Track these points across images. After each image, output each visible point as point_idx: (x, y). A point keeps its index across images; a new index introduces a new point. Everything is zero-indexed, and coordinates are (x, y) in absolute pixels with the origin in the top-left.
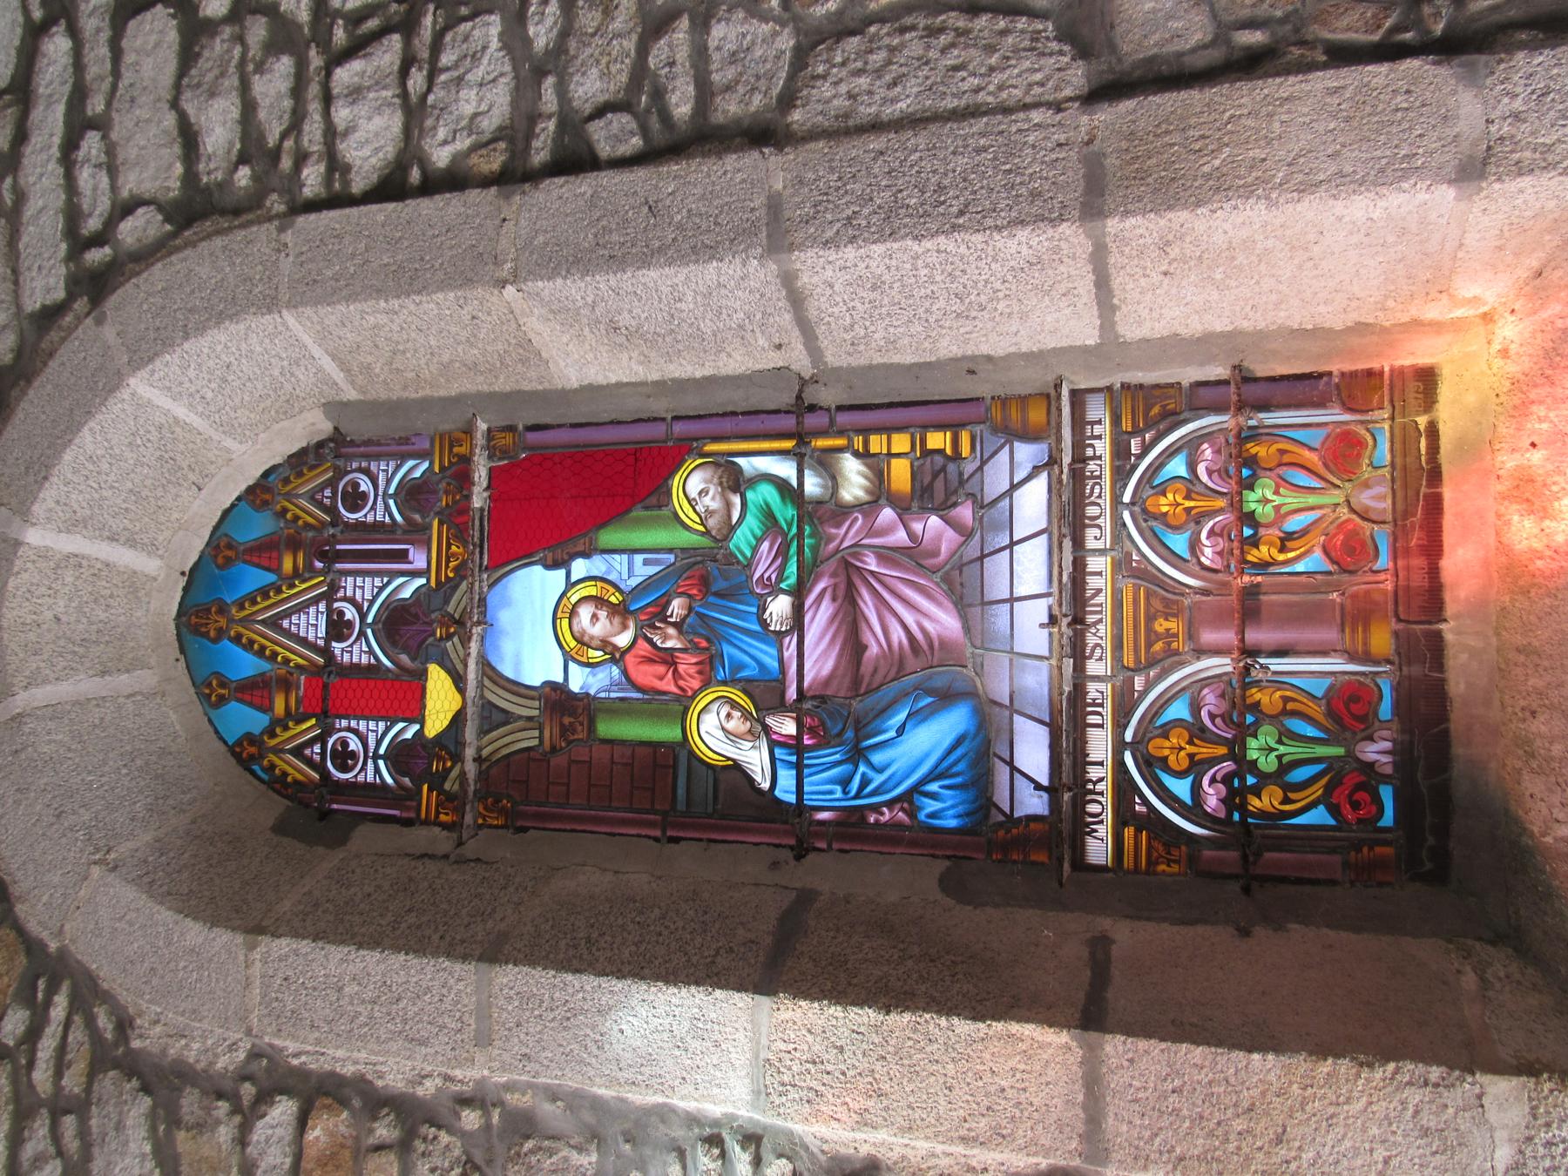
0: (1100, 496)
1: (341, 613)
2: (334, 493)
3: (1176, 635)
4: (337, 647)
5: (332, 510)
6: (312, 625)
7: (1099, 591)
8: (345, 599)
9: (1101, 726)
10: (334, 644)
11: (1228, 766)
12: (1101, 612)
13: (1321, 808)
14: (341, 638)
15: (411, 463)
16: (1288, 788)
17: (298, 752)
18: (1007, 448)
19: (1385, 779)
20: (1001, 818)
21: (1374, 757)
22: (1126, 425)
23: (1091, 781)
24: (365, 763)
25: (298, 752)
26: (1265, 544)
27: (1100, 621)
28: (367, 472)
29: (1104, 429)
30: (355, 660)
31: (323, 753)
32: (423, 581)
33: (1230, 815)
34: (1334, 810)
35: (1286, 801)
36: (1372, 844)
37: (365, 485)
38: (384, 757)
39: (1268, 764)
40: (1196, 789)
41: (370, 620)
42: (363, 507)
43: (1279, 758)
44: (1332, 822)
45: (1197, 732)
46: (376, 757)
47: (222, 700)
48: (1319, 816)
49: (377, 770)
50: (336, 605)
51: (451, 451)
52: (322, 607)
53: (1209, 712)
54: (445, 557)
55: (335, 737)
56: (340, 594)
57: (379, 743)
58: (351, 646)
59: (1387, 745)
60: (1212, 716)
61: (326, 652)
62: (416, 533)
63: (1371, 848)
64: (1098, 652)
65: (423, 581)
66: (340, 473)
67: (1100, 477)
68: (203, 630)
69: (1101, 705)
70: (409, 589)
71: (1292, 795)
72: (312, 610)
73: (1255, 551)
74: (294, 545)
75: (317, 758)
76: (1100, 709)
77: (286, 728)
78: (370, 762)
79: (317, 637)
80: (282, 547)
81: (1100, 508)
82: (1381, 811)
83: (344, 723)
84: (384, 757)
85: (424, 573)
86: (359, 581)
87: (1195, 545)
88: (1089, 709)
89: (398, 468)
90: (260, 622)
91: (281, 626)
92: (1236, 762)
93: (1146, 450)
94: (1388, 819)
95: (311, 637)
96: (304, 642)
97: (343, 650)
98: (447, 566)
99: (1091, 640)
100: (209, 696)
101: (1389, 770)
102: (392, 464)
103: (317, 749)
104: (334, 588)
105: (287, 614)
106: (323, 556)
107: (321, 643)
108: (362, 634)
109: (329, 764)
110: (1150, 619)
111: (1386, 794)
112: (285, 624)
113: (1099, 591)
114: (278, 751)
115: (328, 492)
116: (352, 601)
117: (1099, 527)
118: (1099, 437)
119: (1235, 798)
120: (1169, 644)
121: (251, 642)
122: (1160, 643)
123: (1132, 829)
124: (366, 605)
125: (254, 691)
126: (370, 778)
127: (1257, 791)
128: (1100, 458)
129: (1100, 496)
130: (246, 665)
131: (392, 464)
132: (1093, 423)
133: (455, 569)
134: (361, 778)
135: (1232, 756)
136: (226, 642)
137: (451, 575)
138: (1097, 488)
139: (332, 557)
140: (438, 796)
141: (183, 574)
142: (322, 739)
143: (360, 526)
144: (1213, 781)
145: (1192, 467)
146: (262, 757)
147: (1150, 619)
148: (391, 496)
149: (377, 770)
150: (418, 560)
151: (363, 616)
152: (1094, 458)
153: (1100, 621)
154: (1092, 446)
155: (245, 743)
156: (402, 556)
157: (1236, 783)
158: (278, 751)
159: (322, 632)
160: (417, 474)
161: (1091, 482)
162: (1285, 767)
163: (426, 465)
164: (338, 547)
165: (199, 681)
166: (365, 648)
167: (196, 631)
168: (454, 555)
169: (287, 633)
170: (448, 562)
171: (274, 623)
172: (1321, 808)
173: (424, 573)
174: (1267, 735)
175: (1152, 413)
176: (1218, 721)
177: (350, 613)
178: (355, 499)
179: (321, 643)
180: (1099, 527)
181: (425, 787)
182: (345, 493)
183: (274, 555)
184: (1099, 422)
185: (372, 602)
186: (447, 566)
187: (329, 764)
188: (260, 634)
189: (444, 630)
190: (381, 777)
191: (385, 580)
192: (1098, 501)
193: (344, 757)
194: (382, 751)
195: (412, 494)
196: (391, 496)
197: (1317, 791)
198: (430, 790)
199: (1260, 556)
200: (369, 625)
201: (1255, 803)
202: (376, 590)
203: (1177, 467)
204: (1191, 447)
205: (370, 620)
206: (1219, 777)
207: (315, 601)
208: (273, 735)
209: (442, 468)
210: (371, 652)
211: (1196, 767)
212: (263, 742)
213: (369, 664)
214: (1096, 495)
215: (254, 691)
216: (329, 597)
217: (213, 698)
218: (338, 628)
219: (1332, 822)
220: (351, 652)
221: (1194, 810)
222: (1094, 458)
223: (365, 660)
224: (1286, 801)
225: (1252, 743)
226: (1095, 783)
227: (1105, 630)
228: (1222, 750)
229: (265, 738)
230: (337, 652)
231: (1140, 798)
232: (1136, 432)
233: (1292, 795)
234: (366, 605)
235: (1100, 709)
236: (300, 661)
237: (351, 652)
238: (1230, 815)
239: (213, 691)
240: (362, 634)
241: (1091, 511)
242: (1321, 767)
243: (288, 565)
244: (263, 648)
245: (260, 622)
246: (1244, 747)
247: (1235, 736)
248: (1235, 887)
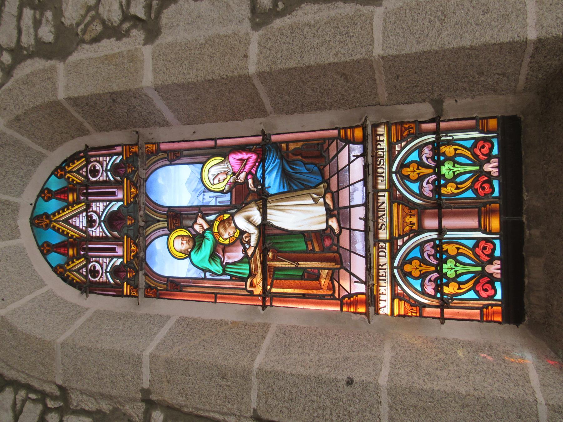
0: (383, 165)
1: (91, 217)
2: (87, 170)
3: (414, 224)
4: (90, 230)
5: (86, 177)
6: (81, 221)
7: (383, 203)
8: (93, 211)
9: (385, 256)
10: (89, 229)
11: (436, 275)
12: (384, 211)
13: (472, 291)
14: (92, 226)
15: (114, 158)
16: (460, 283)
17: (78, 271)
18: (347, 146)
19: (498, 280)
20: (346, 293)
21: (491, 169)
22: (394, 140)
23: (381, 265)
24: (102, 275)
25: (78, 271)
26: (449, 186)
27: (384, 215)
28: (99, 162)
29: (384, 138)
30: (98, 235)
31: (87, 272)
32: (121, 203)
33: (436, 294)
34: (475, 191)
35: (457, 188)
36: (490, 203)
37: (98, 167)
38: (109, 272)
39: (449, 175)
40: (421, 187)
41: (102, 219)
42: (98, 175)
43: (454, 172)
44: (474, 196)
45: (421, 164)
46: (107, 171)
47: (49, 252)
48: (470, 194)
49: (107, 176)
50: (89, 214)
51: (129, 151)
52: (84, 214)
53: (426, 157)
54: (129, 193)
55: (91, 165)
56: (91, 210)
57: (107, 266)
58: (96, 229)
59: (496, 164)
60: (427, 158)
61: (85, 232)
62: (119, 184)
63: (492, 307)
64: (383, 227)
65: (121, 203)
66: (88, 162)
67: (383, 157)
68: (41, 225)
69: (385, 248)
70: (115, 207)
71: (461, 286)
72: (81, 216)
73: (445, 189)
74: (72, 190)
75: (85, 174)
76: (384, 250)
77: (73, 262)
78: (104, 173)
79: (83, 226)
80: (68, 246)
81: (384, 170)
82: (493, 191)
83: (94, 159)
84: (109, 272)
85: (122, 257)
86: (98, 204)
87: (421, 187)
88: (380, 250)
89: (110, 159)
90: (61, 221)
91: (69, 222)
92: (438, 274)
93: (402, 149)
94: (496, 194)
95: (81, 227)
96: (77, 228)
97: (93, 231)
98: (130, 255)
99: (381, 222)
100: (44, 197)
101: (499, 276)
102: (108, 158)
103: (84, 170)
104: (88, 206)
105: (72, 217)
106: (84, 194)
107: (84, 228)
108: (100, 224)
109: (89, 176)
110: (404, 217)
111: (496, 184)
112: (71, 221)
113: (383, 203)
114: (70, 270)
115: (84, 269)
116: (95, 212)
117: (383, 177)
118: (383, 141)
119: (437, 189)
120: (409, 131)
121: (59, 229)
122: (407, 131)
123: (396, 204)
124: (101, 213)
125: (60, 248)
126: (104, 178)
127: (445, 186)
128: (383, 149)
129: (383, 165)
130: (55, 239)
131: (108, 158)
132: (380, 135)
133: (133, 256)
134: (101, 280)
135: (434, 173)
136: (50, 230)
137: (132, 258)
138: (382, 162)
139: (88, 194)
140: (130, 287)
141: (31, 204)
142: (86, 266)
143: (97, 182)
144: (428, 183)
145: (420, 155)
146: (65, 175)
147: (404, 217)
148: (109, 171)
149: (107, 176)
150: (120, 195)
151: (100, 217)
152: (381, 149)
153: (384, 215)
154: (380, 144)
155: (58, 268)
156: (113, 194)
157: (439, 282)
158: (70, 172)
159: (85, 225)
160: (118, 161)
161: (380, 159)
162: (456, 176)
163: (121, 157)
164: (89, 191)
165: (40, 244)
166: (101, 230)
167: (38, 226)
168: (133, 251)
169: (72, 225)
170: (131, 253)
171: (67, 221)
172: (472, 291)
173: (122, 257)
174: (450, 263)
175: (404, 135)
176: (429, 160)
177: (95, 217)
178: (95, 172)
179: (84, 228)
180: (383, 177)
181: (125, 283)
182: (91, 170)
183: (66, 195)
184: (382, 135)
185: (103, 212)
186: (130, 255)
187: (89, 176)
188: (63, 227)
189: (130, 222)
190: (109, 178)
191: (108, 203)
192: (383, 166)
193: (94, 273)
194: (108, 270)
195: (115, 169)
196: (109, 171)
197: (470, 284)
198: (127, 285)
199: (447, 191)
200: (102, 221)
201: (446, 290)
202: (104, 207)
203: (414, 156)
204: (420, 148)
205: (102, 219)
206: (430, 181)
207: (81, 212)
208: (68, 265)
209: (127, 158)
210: (103, 231)
211: (420, 179)
212: (65, 169)
213: (103, 236)
214: (382, 164)
215: (60, 248)
216: (86, 210)
217: (46, 198)
218: (90, 222)
219: (474, 196)
220: (96, 232)
221: (421, 195)
222: (381, 149)
223: (101, 234)
224: (459, 288)
225: (444, 266)
226: (382, 266)
227: (386, 218)
228: (433, 269)
229: (66, 266)
230: (91, 232)
231: (399, 192)
232: (398, 142)
233: (459, 186)
234: (101, 213)
235: (384, 250)
236: (78, 280)
237: (96, 231)
238: (436, 294)
239: (45, 195)
240: (100, 224)
241: (380, 171)
242: (472, 275)
243: (71, 198)
244: (63, 231)
245: (61, 221)
246: (442, 268)
247: (436, 166)
248: (438, 321)
